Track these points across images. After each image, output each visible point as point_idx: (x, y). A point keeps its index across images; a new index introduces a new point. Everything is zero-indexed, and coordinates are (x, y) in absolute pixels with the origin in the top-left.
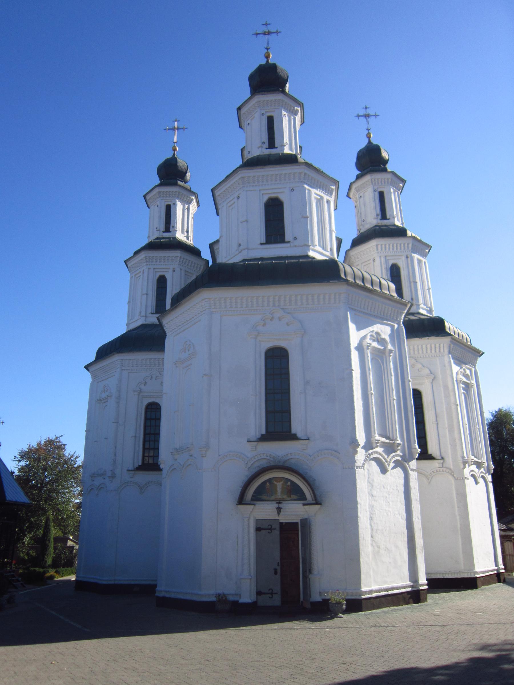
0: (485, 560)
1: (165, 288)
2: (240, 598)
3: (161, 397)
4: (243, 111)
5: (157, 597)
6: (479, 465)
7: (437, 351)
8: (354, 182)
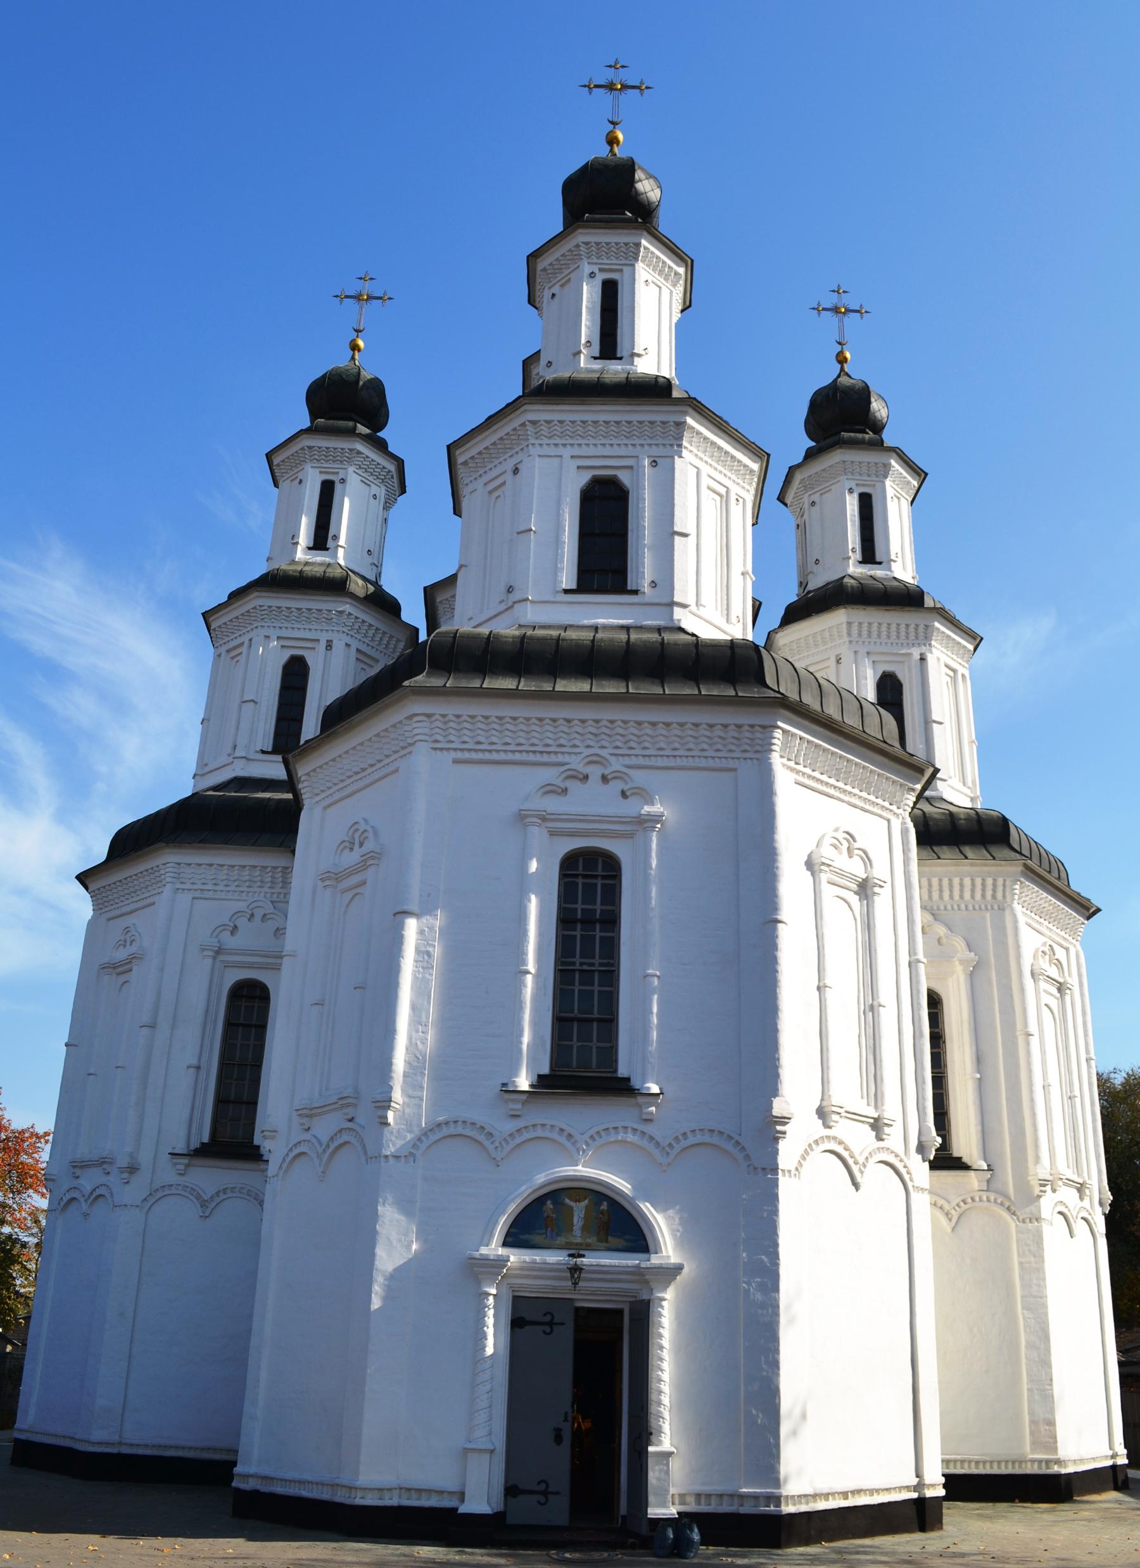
0: (1087, 1436)
1: (303, 689)
2: (462, 1501)
3: (277, 968)
4: (542, 264)
5: (237, 1490)
6: (1081, 1189)
7: (989, 893)
8: (799, 466)
